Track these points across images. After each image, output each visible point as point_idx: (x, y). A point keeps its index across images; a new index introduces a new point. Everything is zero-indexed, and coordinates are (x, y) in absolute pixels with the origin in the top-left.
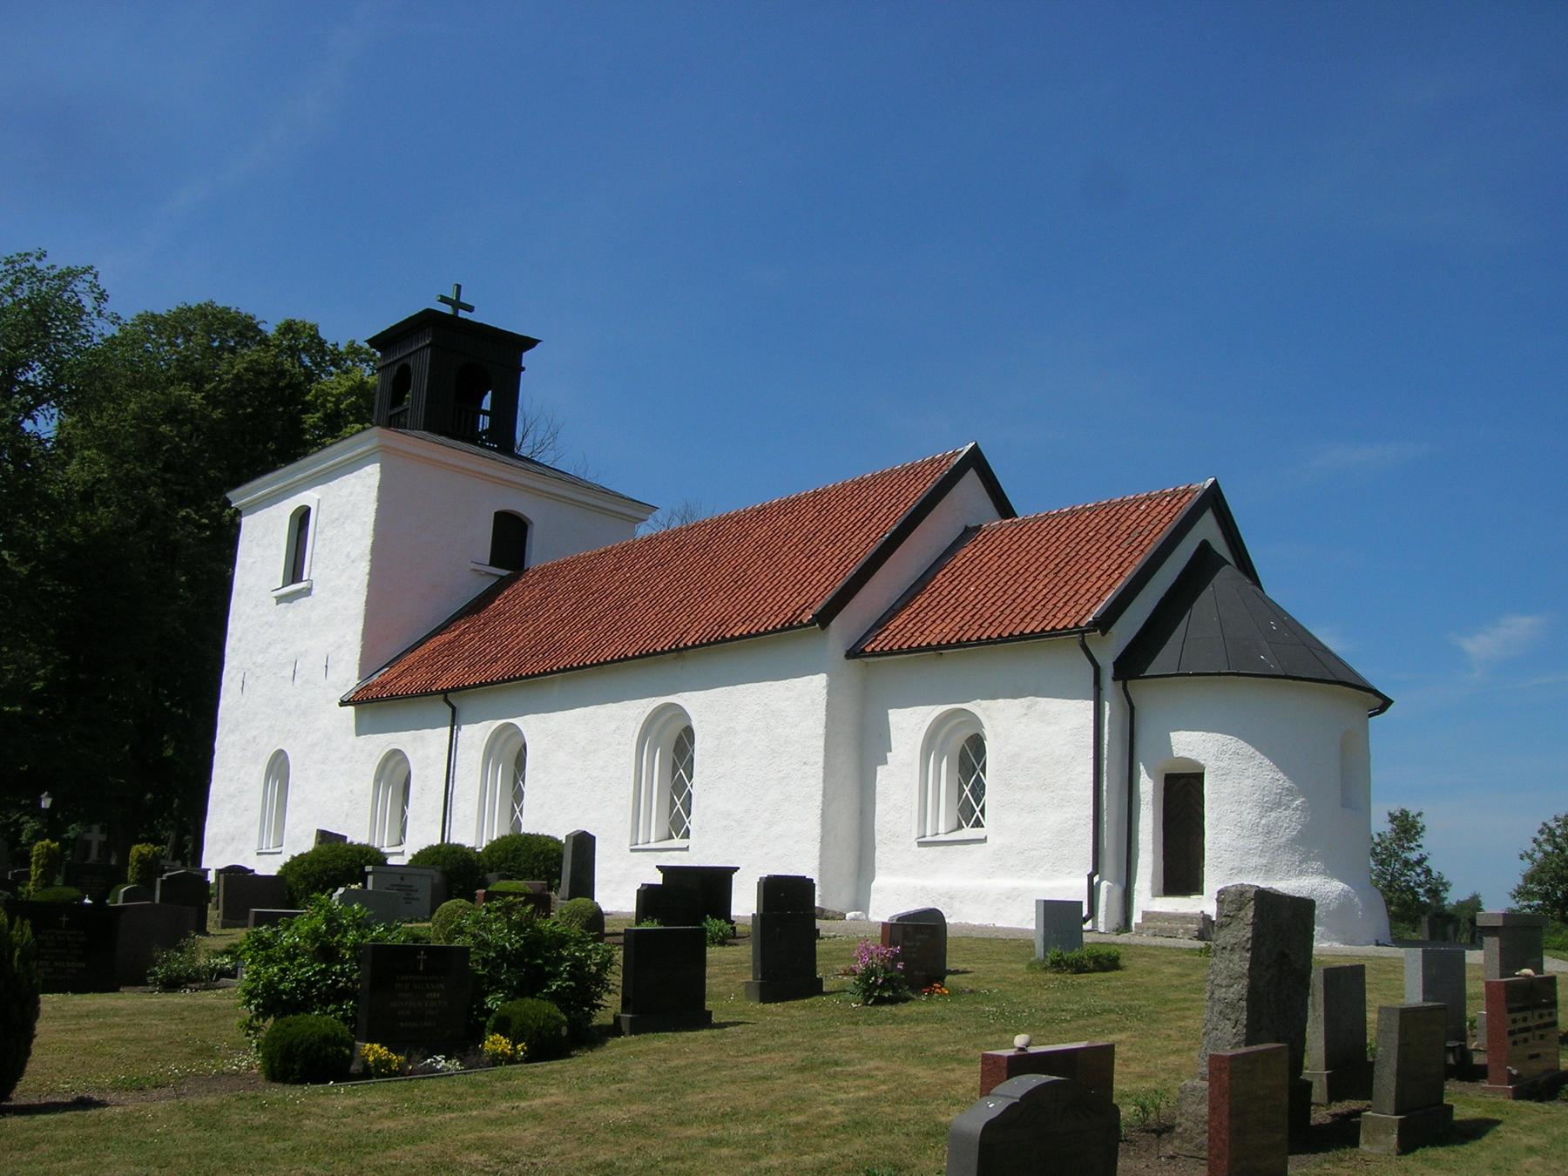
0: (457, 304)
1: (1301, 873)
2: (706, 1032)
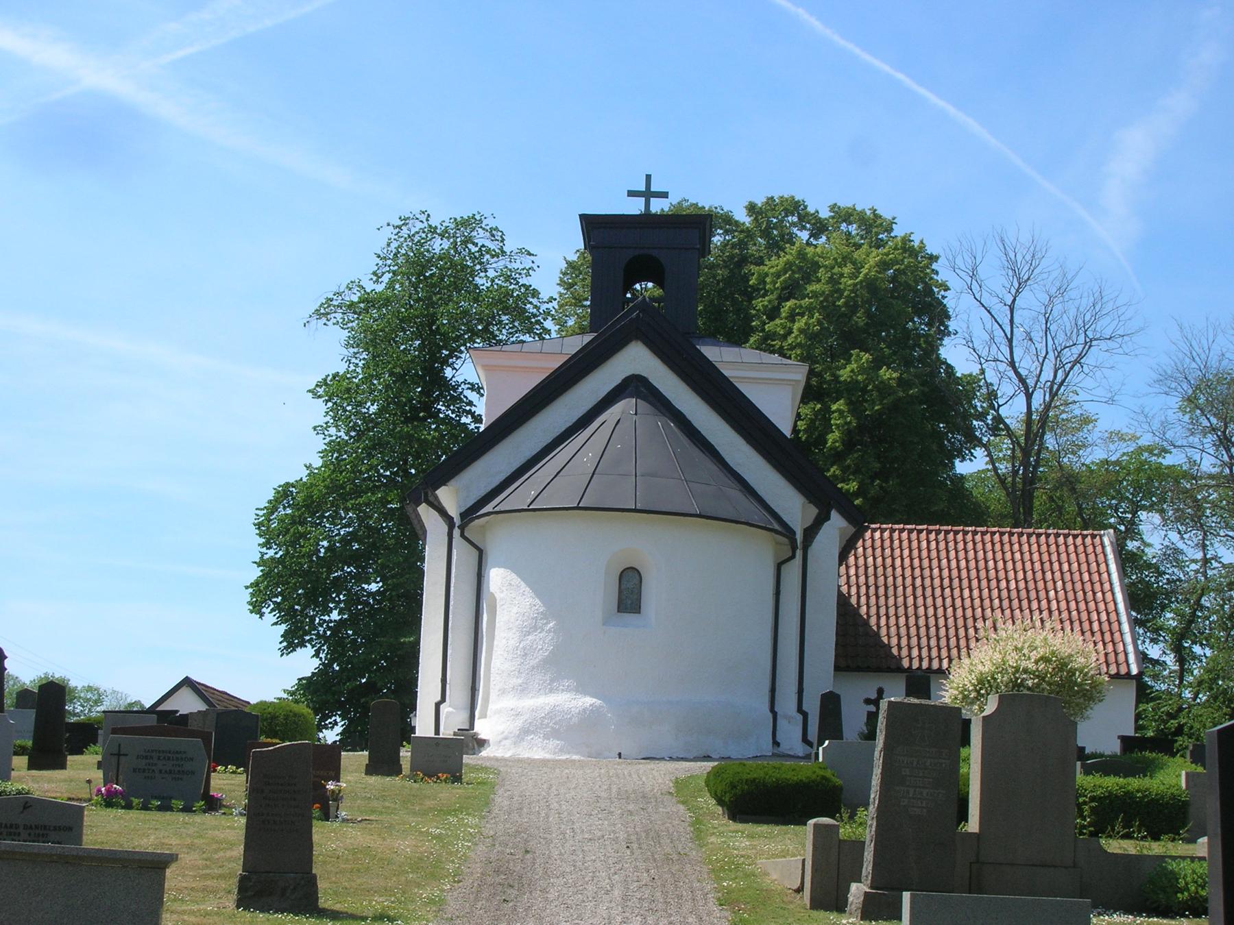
0: (648, 194)
1: (551, 691)
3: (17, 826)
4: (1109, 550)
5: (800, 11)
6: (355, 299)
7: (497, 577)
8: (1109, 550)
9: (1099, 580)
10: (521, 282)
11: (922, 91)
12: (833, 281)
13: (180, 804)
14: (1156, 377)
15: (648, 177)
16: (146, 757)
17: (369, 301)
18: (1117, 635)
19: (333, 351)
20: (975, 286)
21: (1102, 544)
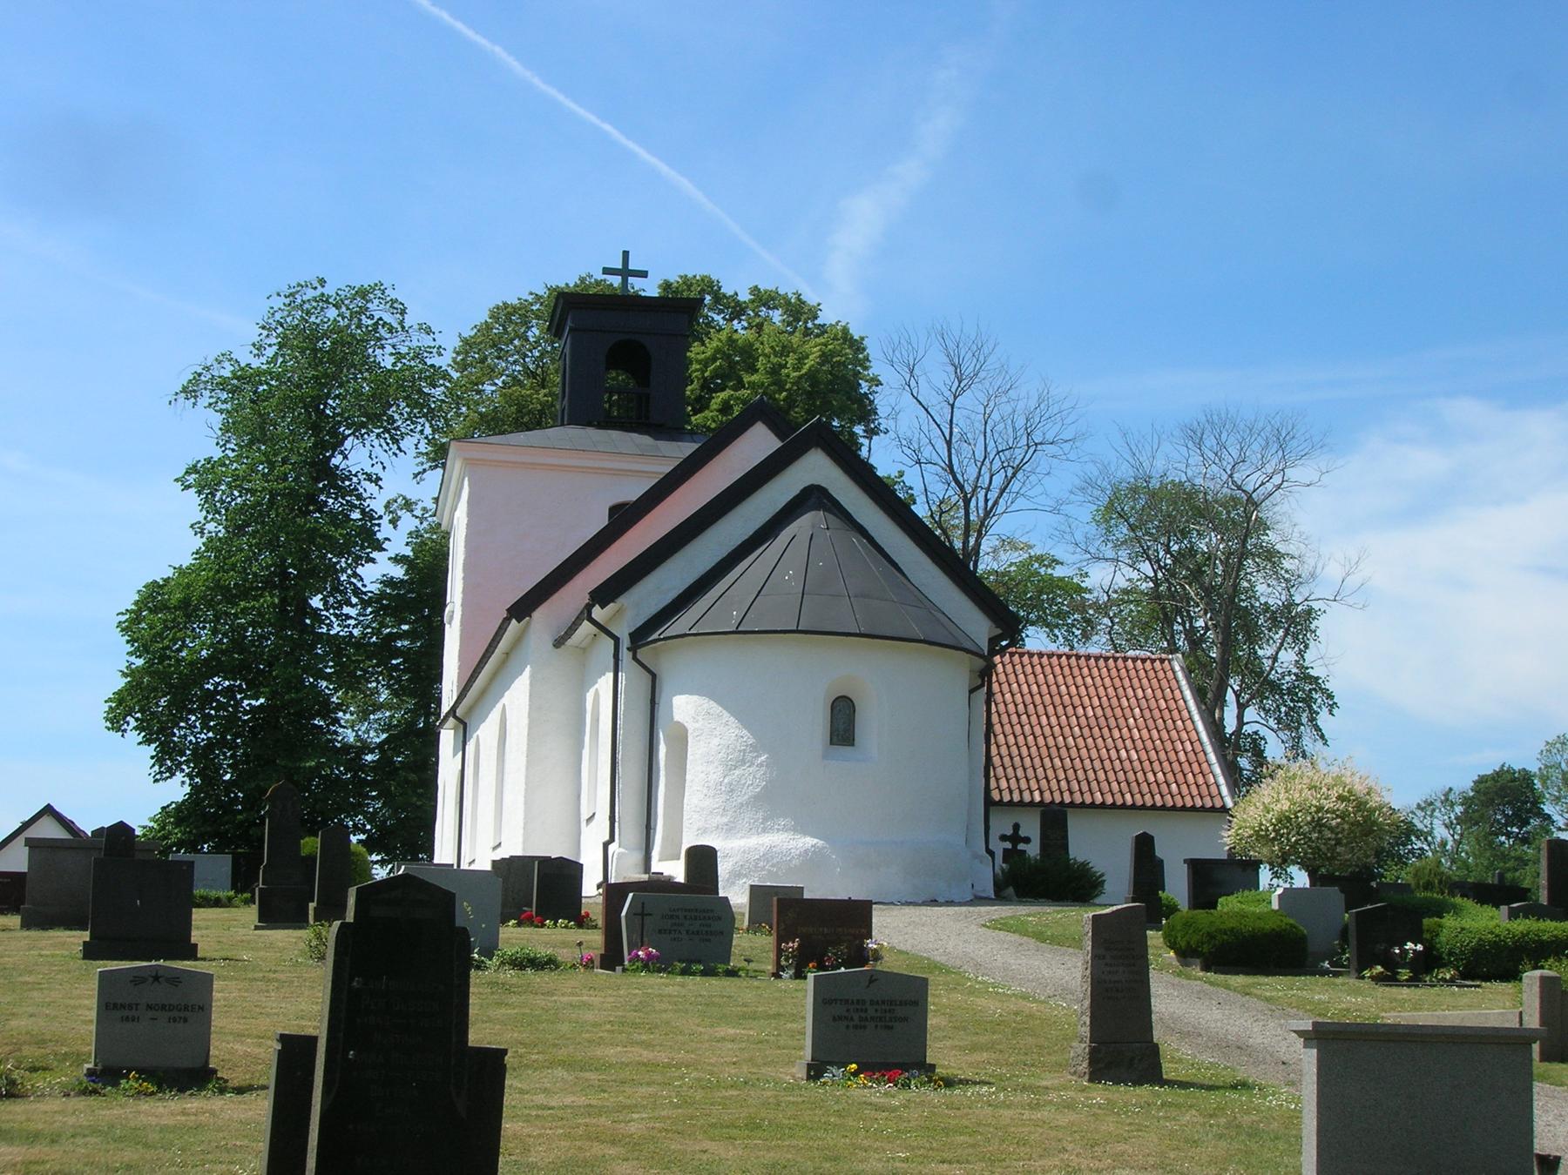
0: (625, 272)
1: (764, 831)
2: (1145, 1091)
3: (864, 1002)
4: (1180, 675)
5: (497, 49)
6: (227, 373)
7: (684, 707)
8: (1180, 675)
9: (1175, 707)
10: (429, 362)
11: (631, 145)
12: (775, 371)
13: (680, 965)
14: (1077, 482)
15: (626, 254)
16: (672, 917)
17: (245, 377)
18: (1205, 766)
19: (202, 434)
20: (913, 383)
21: (1172, 669)
